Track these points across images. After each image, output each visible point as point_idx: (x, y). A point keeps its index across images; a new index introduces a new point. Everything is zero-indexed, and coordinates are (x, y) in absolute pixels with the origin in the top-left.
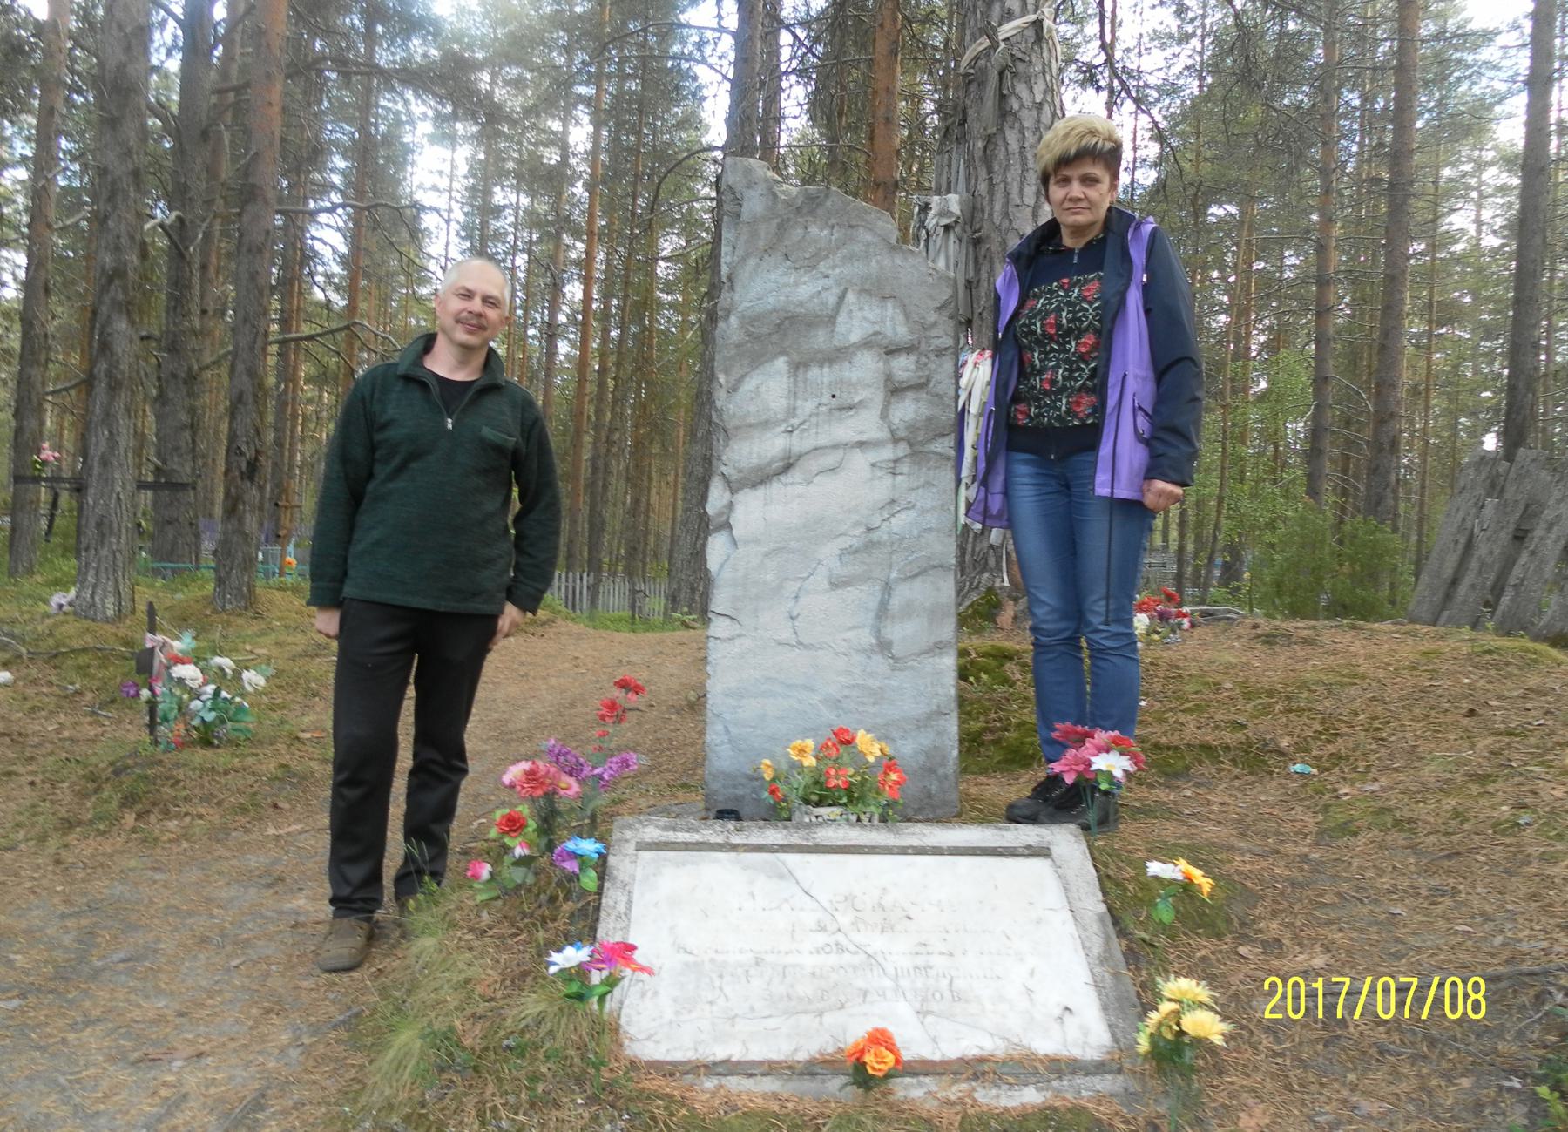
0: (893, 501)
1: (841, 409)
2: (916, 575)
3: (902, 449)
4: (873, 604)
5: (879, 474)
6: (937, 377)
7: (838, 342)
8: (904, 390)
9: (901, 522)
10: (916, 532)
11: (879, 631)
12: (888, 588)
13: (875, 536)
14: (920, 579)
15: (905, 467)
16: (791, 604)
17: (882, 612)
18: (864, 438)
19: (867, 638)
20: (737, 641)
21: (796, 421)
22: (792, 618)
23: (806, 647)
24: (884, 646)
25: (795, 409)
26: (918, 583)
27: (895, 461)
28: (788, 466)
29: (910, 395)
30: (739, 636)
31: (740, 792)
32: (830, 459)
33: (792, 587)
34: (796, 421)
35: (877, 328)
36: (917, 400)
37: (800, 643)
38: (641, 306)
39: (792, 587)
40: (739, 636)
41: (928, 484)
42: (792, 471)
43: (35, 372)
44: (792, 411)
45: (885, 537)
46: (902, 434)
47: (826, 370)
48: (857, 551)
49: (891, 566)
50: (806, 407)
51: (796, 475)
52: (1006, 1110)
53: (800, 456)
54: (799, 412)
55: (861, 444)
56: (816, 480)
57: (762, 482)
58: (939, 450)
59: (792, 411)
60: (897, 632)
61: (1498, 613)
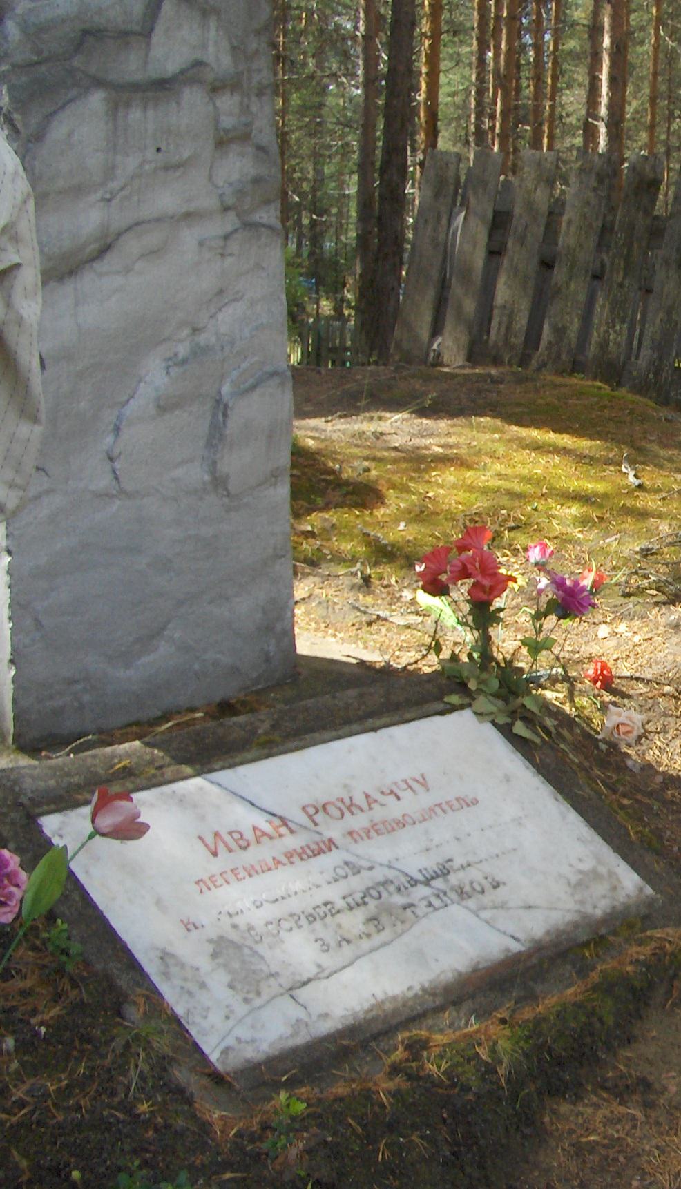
0: (221, 292)
1: (167, 168)
2: (253, 387)
4: (203, 428)
6: (257, 124)
7: (153, 72)
9: (228, 318)
10: (247, 333)
11: (214, 463)
13: (202, 339)
14: (258, 391)
15: (234, 246)
16: (110, 439)
17: (216, 436)
18: (192, 207)
19: (197, 474)
22: (111, 459)
24: (219, 482)
25: (113, 168)
26: (255, 396)
30: (48, 492)
32: (153, 238)
33: (109, 416)
35: (198, 55)
37: (122, 491)
39: (109, 416)
40: (48, 492)
41: (259, 266)
42: (108, 257)
44: (110, 171)
45: (213, 340)
46: (230, 201)
47: (151, 113)
48: (184, 362)
50: (130, 163)
51: (111, 261)
52: (493, 417)
55: (188, 216)
56: (138, 266)
58: (265, 220)
59: (110, 171)
61: (43, 417)
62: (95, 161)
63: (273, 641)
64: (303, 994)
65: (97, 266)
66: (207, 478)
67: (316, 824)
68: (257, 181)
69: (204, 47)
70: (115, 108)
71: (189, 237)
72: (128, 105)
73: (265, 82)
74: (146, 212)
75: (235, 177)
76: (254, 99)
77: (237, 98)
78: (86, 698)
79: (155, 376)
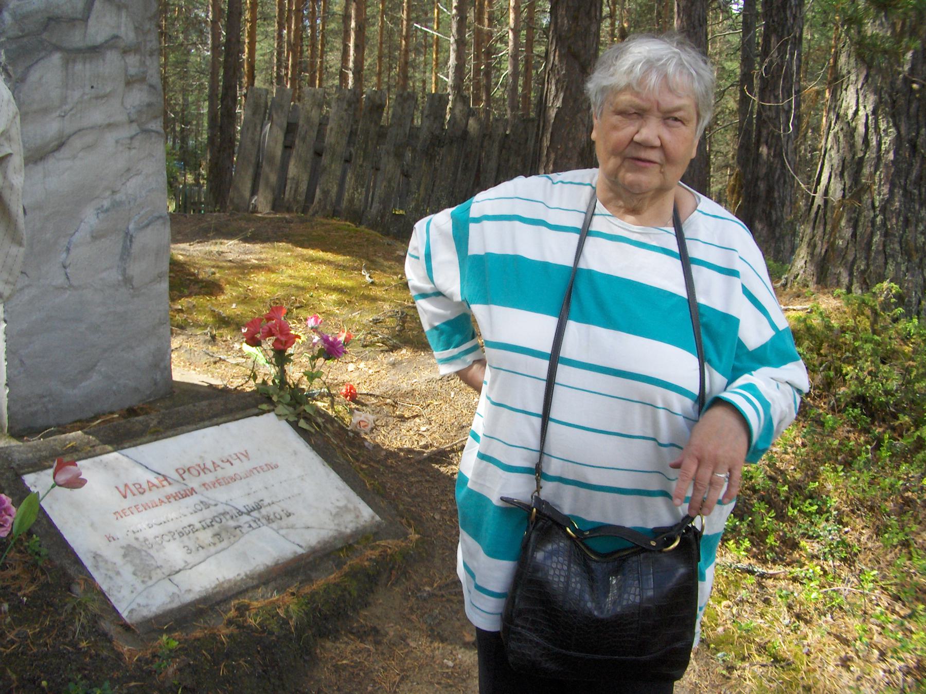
2: (147, 225)
3: (135, 129)
5: (120, 148)
6: (150, 72)
7: (89, 42)
8: (134, 82)
11: (125, 269)
12: (129, 237)
13: (118, 197)
15: (136, 143)
16: (64, 255)
17: (126, 254)
18: (112, 121)
19: (114, 276)
20: (26, 291)
21: (67, 107)
22: (65, 267)
23: (75, 288)
24: (127, 281)
25: (66, 98)
26: (149, 230)
27: (132, 138)
28: (61, 144)
29: (137, 86)
30: (28, 286)
31: (34, 409)
32: (89, 138)
33: (64, 242)
34: (67, 107)
35: (115, 32)
36: (141, 90)
37: (71, 286)
38: (852, 146)
39: (64, 242)
41: (151, 155)
42: (63, 149)
43: (888, 205)
44: (64, 100)
45: (124, 198)
47: (88, 66)
48: (107, 210)
49: (129, 219)
51: (65, 152)
53: (69, 137)
54: (69, 100)
55: (110, 126)
57: (42, 159)
59: (64, 100)
60: (136, 269)
62: (55, 94)
65: (56, 154)
66: (120, 278)
68: (149, 105)
69: (119, 27)
73: (154, 48)
78: (50, 406)
79: (90, 219)
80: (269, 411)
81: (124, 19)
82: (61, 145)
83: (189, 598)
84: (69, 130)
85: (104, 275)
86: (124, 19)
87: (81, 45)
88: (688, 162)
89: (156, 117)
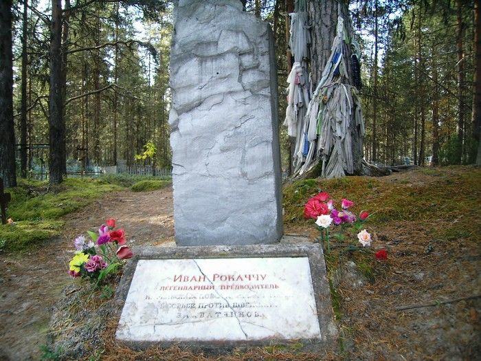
1: (221, 78)
18: (232, 90)
23: (213, 176)
25: (202, 79)
26: (256, 148)
30: (185, 173)
31: (189, 236)
35: (235, 45)
40: (185, 173)
41: (260, 108)
44: (200, 80)
47: (214, 63)
55: (230, 93)
59: (200, 80)
62: (195, 78)
63: (268, 230)
64: (158, 327)
65: (199, 108)
66: (240, 173)
67: (214, 280)
68: (259, 81)
69: (238, 42)
70: (201, 62)
71: (231, 100)
72: (206, 61)
73: (264, 51)
74: (215, 91)
75: (251, 80)
76: (260, 57)
77: (251, 56)
78: (198, 236)
79: (220, 140)
80: (305, 256)
81: (240, 38)
82: (200, 104)
83: (133, 338)
84: (203, 96)
85: (229, 171)
86: (240, 38)
87: (214, 54)
88: (175, 160)
89: (265, 88)
